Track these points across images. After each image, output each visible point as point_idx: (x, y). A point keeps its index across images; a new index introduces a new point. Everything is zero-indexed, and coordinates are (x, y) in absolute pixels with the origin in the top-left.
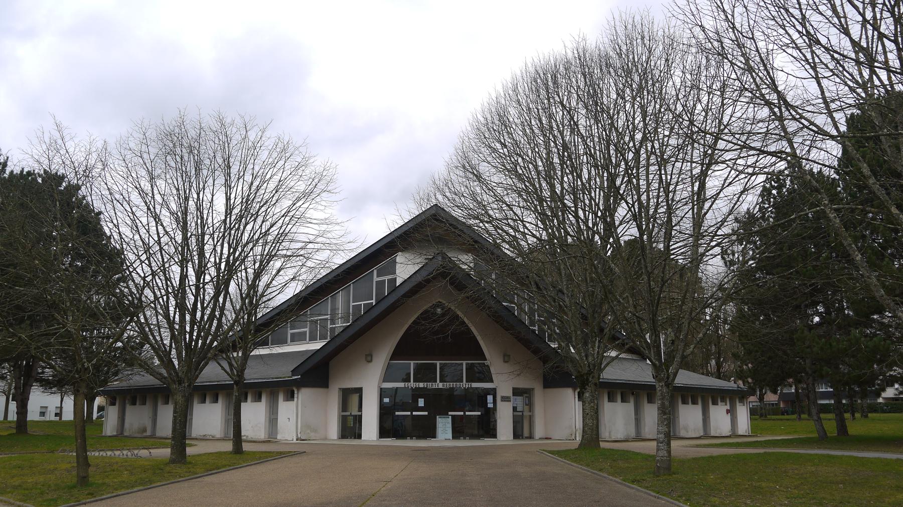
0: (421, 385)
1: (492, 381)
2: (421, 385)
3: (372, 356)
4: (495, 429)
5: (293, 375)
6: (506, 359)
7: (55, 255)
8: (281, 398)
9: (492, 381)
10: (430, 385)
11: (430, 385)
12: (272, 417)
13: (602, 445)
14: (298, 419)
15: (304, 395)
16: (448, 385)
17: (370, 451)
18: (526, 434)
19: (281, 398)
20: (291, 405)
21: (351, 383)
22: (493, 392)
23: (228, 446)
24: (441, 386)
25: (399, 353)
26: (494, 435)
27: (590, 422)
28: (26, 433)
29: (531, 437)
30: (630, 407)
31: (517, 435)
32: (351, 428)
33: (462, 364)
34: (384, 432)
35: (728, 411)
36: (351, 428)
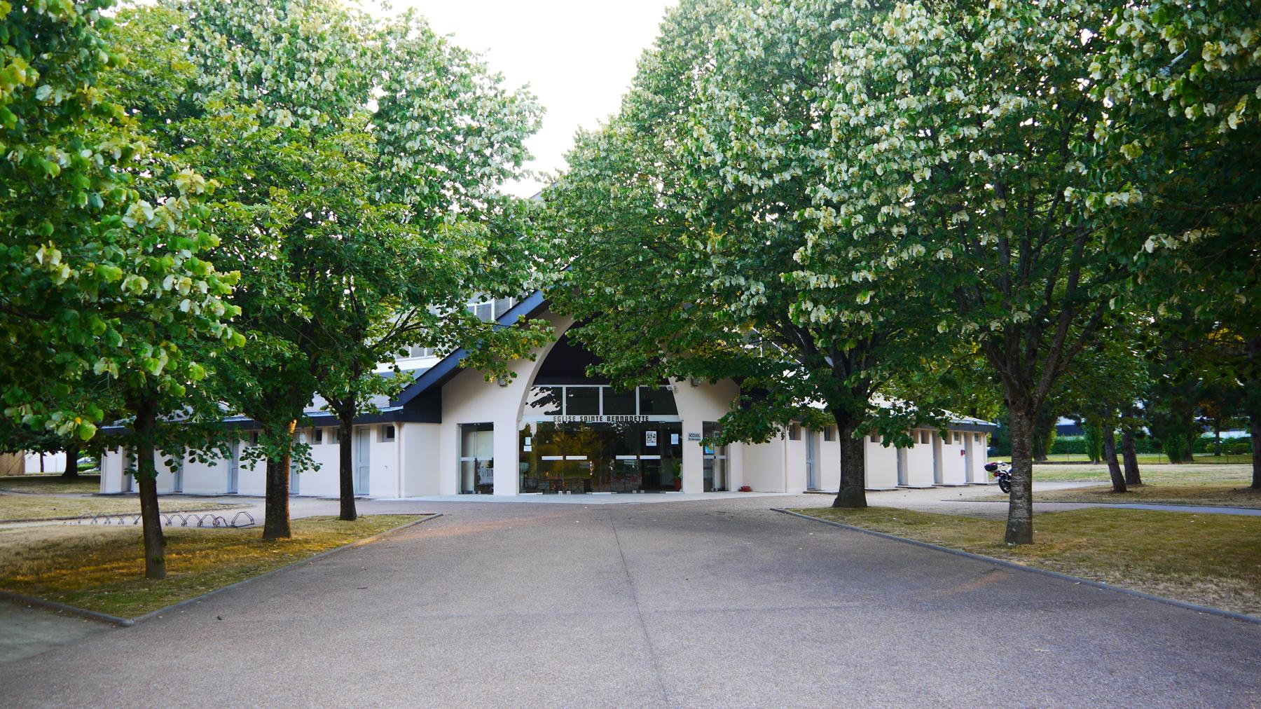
0: (578, 418)
1: (674, 411)
2: (578, 418)
11: (589, 419)
13: (871, 499)
15: (407, 433)
17: (508, 508)
18: (717, 484)
19: (374, 435)
20: (389, 446)
21: (474, 414)
22: (677, 428)
23: (335, 509)
24: (605, 419)
25: (541, 378)
26: (676, 485)
27: (850, 468)
29: (723, 489)
31: (708, 486)
32: (478, 480)
34: (527, 485)
35: (963, 452)
36: (478, 480)
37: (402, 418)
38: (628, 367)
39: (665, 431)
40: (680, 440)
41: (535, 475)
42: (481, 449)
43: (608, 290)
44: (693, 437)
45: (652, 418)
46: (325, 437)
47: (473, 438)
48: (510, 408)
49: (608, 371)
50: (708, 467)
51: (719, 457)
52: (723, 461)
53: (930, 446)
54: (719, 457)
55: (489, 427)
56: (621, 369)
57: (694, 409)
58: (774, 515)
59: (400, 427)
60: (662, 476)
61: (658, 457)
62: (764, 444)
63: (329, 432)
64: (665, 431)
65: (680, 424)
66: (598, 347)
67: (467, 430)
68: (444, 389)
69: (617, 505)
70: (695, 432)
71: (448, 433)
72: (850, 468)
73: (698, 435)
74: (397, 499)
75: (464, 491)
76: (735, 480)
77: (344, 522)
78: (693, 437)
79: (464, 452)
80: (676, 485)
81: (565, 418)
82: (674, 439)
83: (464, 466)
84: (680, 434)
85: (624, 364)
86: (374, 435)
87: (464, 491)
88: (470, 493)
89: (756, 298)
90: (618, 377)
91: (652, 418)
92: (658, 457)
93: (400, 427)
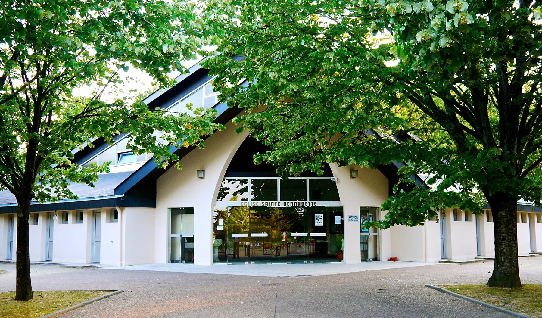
1: (338, 199)
3: (204, 171)
4: (342, 252)
5: (116, 194)
6: (353, 173)
7: (218, 71)
8: (55, 218)
9: (338, 199)
10: (269, 204)
11: (269, 204)
12: (95, 240)
14: (129, 244)
15: (128, 214)
16: (289, 204)
18: (371, 255)
19: (104, 217)
20: (115, 226)
22: (339, 211)
24: (282, 204)
25: (235, 169)
26: (338, 256)
28: (520, 285)
29: (376, 259)
30: (472, 224)
31: (365, 257)
33: (305, 180)
34: (222, 256)
37: (123, 203)
38: (294, 154)
39: (330, 214)
40: (342, 221)
41: (227, 250)
42: (189, 226)
43: (271, 75)
44: (352, 218)
45: (319, 203)
46: (70, 217)
47: (182, 219)
48: (206, 195)
49: (275, 157)
50: (364, 242)
51: (373, 234)
52: (375, 237)
53: (527, 224)
54: (373, 234)
55: (190, 211)
56: (286, 156)
57: (353, 195)
58: (434, 297)
59: (122, 210)
60: (327, 250)
61: (324, 235)
62: (418, 226)
63: (73, 214)
64: (330, 214)
65: (342, 208)
66: (268, 142)
67: (175, 212)
68: (158, 181)
69: (287, 278)
70: (354, 215)
71: (161, 214)
72: (504, 249)
73: (356, 217)
74: (119, 268)
75: (173, 261)
76: (385, 252)
77: (19, 304)
78: (352, 218)
79: (173, 230)
80: (338, 256)
81: (250, 204)
82: (337, 220)
83: (173, 240)
84: (342, 216)
85: (289, 150)
86: (104, 217)
87: (173, 261)
88: (177, 262)
89: (458, 16)
90: (284, 164)
91: (319, 203)
92: (324, 235)
93: (122, 210)
